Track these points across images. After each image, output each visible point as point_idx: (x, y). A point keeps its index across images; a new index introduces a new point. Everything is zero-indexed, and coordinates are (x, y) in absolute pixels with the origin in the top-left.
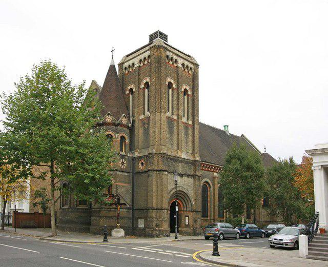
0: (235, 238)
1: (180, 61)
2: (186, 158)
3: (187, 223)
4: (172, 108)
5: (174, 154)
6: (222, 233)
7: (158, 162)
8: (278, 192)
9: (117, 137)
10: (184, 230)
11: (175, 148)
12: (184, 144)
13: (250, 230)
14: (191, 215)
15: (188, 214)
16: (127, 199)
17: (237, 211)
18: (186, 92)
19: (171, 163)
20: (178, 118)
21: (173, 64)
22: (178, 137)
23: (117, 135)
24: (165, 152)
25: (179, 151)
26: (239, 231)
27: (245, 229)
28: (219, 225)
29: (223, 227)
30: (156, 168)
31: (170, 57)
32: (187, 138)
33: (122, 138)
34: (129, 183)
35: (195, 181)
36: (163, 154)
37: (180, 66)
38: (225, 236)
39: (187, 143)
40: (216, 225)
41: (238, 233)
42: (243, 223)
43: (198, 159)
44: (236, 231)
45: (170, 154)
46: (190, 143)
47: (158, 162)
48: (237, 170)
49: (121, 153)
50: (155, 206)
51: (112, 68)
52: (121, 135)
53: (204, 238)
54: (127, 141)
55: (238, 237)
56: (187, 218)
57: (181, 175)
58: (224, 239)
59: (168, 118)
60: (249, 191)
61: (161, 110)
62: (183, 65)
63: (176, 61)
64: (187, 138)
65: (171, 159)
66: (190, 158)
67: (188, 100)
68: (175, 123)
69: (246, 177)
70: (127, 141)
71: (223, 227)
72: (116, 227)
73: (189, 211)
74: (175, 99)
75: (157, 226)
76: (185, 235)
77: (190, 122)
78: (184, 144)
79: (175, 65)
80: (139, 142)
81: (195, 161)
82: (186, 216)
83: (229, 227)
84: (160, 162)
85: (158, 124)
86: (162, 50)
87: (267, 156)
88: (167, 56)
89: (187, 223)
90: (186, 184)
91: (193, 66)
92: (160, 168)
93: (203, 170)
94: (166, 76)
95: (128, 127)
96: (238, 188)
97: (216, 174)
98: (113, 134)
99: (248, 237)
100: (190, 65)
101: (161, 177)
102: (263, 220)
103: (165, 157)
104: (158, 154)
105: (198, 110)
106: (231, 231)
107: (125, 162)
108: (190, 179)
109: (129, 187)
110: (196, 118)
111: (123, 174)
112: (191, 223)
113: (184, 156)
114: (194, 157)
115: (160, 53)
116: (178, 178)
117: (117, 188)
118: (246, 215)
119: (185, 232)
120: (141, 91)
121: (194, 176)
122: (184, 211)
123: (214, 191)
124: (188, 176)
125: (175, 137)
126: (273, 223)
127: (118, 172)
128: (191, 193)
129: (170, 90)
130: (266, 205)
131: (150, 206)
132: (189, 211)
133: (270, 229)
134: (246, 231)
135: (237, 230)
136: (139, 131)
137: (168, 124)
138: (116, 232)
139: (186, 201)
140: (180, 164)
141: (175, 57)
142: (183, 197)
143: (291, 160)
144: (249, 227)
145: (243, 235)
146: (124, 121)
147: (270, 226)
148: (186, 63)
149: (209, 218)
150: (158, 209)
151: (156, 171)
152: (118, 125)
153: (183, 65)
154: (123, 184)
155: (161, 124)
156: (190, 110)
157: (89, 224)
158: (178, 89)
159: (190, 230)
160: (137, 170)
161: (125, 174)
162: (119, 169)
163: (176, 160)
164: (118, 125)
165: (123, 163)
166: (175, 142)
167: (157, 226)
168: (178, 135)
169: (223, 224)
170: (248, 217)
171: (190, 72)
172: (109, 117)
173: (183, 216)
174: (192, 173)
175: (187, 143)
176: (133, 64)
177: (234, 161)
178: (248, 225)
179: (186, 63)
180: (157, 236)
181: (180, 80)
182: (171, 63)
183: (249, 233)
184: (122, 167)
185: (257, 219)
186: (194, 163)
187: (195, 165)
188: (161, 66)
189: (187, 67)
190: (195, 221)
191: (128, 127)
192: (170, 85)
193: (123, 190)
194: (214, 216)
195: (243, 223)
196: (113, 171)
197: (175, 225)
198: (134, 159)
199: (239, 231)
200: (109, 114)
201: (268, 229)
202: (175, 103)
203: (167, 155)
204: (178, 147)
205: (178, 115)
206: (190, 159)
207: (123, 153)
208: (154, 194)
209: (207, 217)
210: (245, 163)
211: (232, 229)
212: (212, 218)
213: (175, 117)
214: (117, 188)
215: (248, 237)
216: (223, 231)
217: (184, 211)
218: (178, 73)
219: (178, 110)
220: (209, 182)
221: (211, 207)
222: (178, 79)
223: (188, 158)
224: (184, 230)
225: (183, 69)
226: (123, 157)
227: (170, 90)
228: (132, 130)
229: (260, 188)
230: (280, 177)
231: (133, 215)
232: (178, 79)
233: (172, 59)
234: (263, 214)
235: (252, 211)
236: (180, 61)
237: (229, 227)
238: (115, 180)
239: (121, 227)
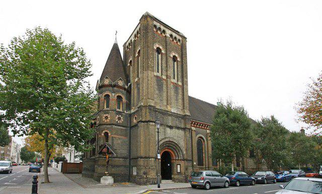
0: (225, 187)
1: (168, 32)
2: (176, 112)
3: (179, 171)
4: (162, 69)
5: (163, 108)
6: (208, 182)
7: (146, 113)
8: (263, 145)
9: (113, 96)
10: (176, 177)
11: (165, 104)
12: (173, 101)
13: (240, 177)
14: (182, 163)
15: (180, 162)
16: (123, 151)
17: (228, 159)
18: (175, 58)
19: (159, 116)
20: (167, 78)
21: (161, 33)
22: (167, 94)
23: (113, 94)
24: (153, 105)
25: (168, 106)
26: (228, 179)
27: (234, 176)
28: (205, 173)
29: (209, 175)
30: (143, 120)
31: (158, 27)
32: (177, 96)
33: (119, 97)
34: (126, 136)
35: (185, 133)
36: (150, 106)
37: (168, 35)
38: (213, 185)
39: (177, 100)
40: (202, 173)
41: (227, 181)
42: (233, 171)
43: (188, 114)
44: (224, 180)
45: (158, 107)
46: (180, 101)
47: (146, 113)
48: (224, 122)
49: (118, 110)
50: (143, 155)
51: (115, 48)
52: (118, 95)
53: (189, 185)
54: (124, 100)
55: (227, 185)
56: (179, 166)
57: (171, 127)
58: (211, 188)
59: (157, 77)
60: (237, 140)
61: (148, 68)
62: (171, 36)
63: (164, 31)
64: (177, 96)
65: (159, 112)
66: (181, 113)
67: (177, 65)
68: (165, 83)
69: (234, 128)
70: (124, 100)
71: (209, 175)
72: (105, 175)
73: (181, 160)
74: (164, 62)
75: (145, 173)
76: (178, 182)
77: (180, 83)
78: (173, 101)
79: (163, 35)
80: (134, 101)
81: (185, 115)
82: (177, 165)
83: (216, 176)
84: (148, 114)
85: (145, 81)
86: (149, 19)
87: (251, 119)
88: (155, 26)
89: (179, 171)
90: (176, 135)
91: (181, 38)
92: (148, 120)
93: (202, 128)
94: (154, 42)
95: (125, 89)
96: (228, 139)
97: (208, 131)
98: (110, 94)
99: (238, 184)
100: (178, 37)
101: (148, 128)
102: (250, 167)
103: (153, 109)
104: (145, 106)
105: (186, 73)
106: (219, 179)
107: (122, 118)
108: (181, 131)
109: (127, 139)
110: (185, 80)
111: (120, 127)
112: (183, 171)
113: (173, 111)
114: (185, 112)
115: (148, 21)
116: (168, 130)
117: (113, 140)
118: (236, 164)
119: (177, 179)
120: (136, 59)
121: (184, 129)
122: (176, 160)
123: (208, 145)
124: (178, 128)
125: (165, 94)
126: (259, 171)
127: (114, 126)
128: (182, 144)
129: (160, 55)
130: (252, 156)
131: (139, 155)
132: (181, 160)
133: (259, 176)
134: (235, 179)
135: (226, 178)
136: (134, 92)
137: (157, 82)
138: (105, 179)
139: (178, 151)
140: (170, 118)
141: (162, 28)
142: (174, 147)
143: (272, 117)
144: (239, 175)
145: (232, 184)
146: (121, 83)
147: (258, 173)
148: (174, 35)
149: (204, 166)
150: (146, 158)
151: (144, 122)
152: (115, 86)
153: (171, 36)
154: (120, 137)
155: (148, 80)
156: (180, 74)
157: (94, 171)
158: (166, 54)
159: (181, 177)
160: (133, 124)
161: (122, 128)
162: (115, 123)
163: (165, 113)
164: (115, 86)
165: (119, 119)
166: (165, 98)
167: (145, 173)
168: (167, 92)
169: (209, 172)
170: (238, 165)
171: (179, 43)
172: (107, 80)
173: (175, 165)
174: (183, 126)
175: (177, 100)
176: (131, 40)
177: (221, 115)
178: (237, 173)
179: (174, 35)
180: (145, 184)
181: (168, 47)
182: (159, 32)
183: (239, 181)
184: (119, 122)
185: (245, 167)
186: (184, 117)
187: (185, 120)
188: (148, 32)
189: (175, 38)
190: (186, 169)
191: (125, 89)
192: (159, 51)
193: (119, 141)
194: (208, 165)
195: (233, 171)
196: (110, 124)
197: (167, 173)
198: (130, 115)
199: (228, 179)
200: (107, 78)
201: (256, 176)
202: (164, 65)
203: (154, 107)
204: (167, 102)
205: (167, 76)
206: (180, 114)
207: (121, 110)
208: (142, 144)
209: (203, 165)
210: (232, 116)
211: (220, 177)
212: (207, 166)
213: (164, 77)
214: (113, 140)
215: (238, 184)
216: (209, 179)
217: (176, 160)
218: (166, 42)
219: (167, 71)
220: (203, 137)
221: (205, 157)
222: (166, 46)
223: (179, 113)
224: (176, 177)
225: (171, 39)
226: (119, 113)
227: (160, 55)
228: (129, 91)
229: (247, 138)
230: (264, 132)
231: (130, 164)
232: (166, 46)
233: (160, 29)
234: (250, 163)
235: (241, 159)
236: (168, 32)
237: (216, 176)
238: (111, 132)
239: (110, 175)
